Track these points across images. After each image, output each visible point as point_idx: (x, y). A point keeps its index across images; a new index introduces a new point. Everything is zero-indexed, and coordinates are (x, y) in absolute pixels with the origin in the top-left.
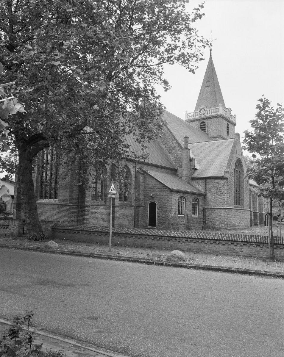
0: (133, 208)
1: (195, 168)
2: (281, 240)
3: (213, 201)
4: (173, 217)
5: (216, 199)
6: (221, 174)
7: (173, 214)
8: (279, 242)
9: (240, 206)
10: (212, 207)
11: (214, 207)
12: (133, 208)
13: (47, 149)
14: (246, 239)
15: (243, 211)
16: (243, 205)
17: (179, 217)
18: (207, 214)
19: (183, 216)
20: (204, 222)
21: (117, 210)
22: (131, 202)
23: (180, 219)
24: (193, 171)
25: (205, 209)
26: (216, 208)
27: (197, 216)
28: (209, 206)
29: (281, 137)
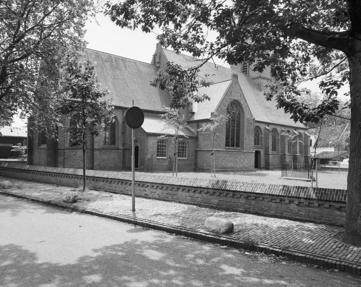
0: (121, 151)
1: (193, 111)
2: (342, 196)
3: (204, 144)
4: (149, 159)
5: (205, 141)
6: (208, 117)
7: (150, 156)
8: (333, 198)
9: (239, 148)
10: (202, 149)
11: (204, 149)
12: (121, 151)
13: (289, 56)
14: (339, 198)
15: (242, 153)
16: (243, 147)
17: (159, 159)
18: (198, 157)
19: (187, 158)
20: (196, 164)
21: (96, 153)
22: (118, 145)
23: (160, 161)
24: (190, 115)
25: (196, 152)
26: (205, 150)
27: (187, 158)
28: (200, 148)
29: (341, 55)
